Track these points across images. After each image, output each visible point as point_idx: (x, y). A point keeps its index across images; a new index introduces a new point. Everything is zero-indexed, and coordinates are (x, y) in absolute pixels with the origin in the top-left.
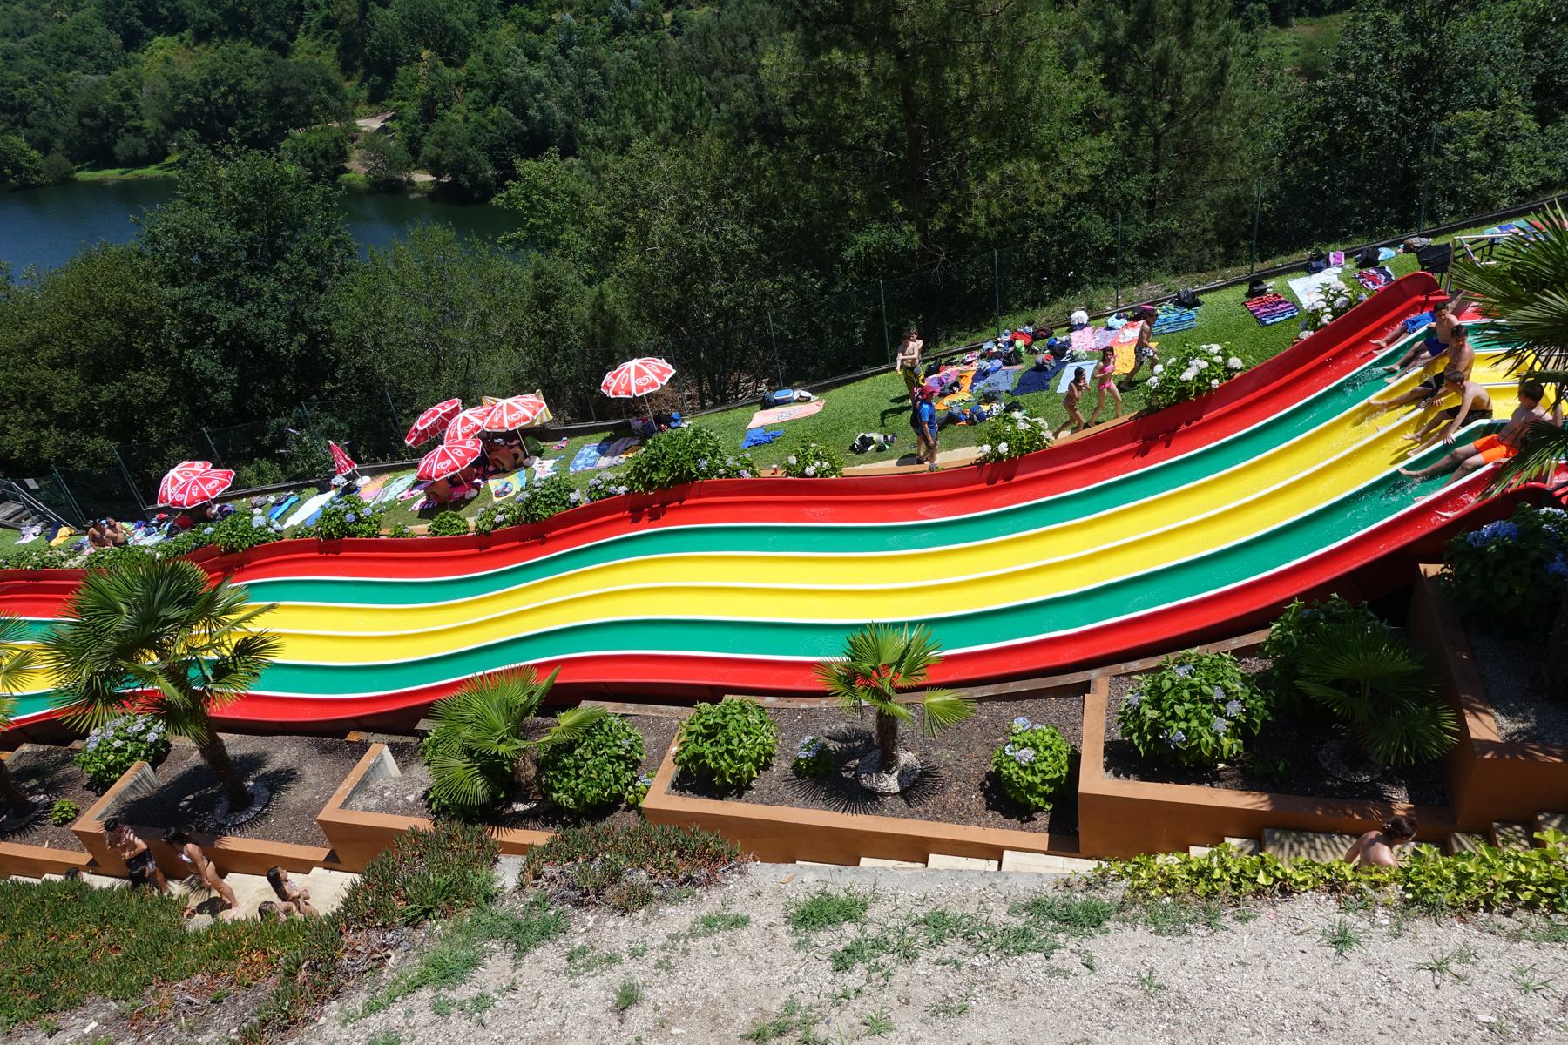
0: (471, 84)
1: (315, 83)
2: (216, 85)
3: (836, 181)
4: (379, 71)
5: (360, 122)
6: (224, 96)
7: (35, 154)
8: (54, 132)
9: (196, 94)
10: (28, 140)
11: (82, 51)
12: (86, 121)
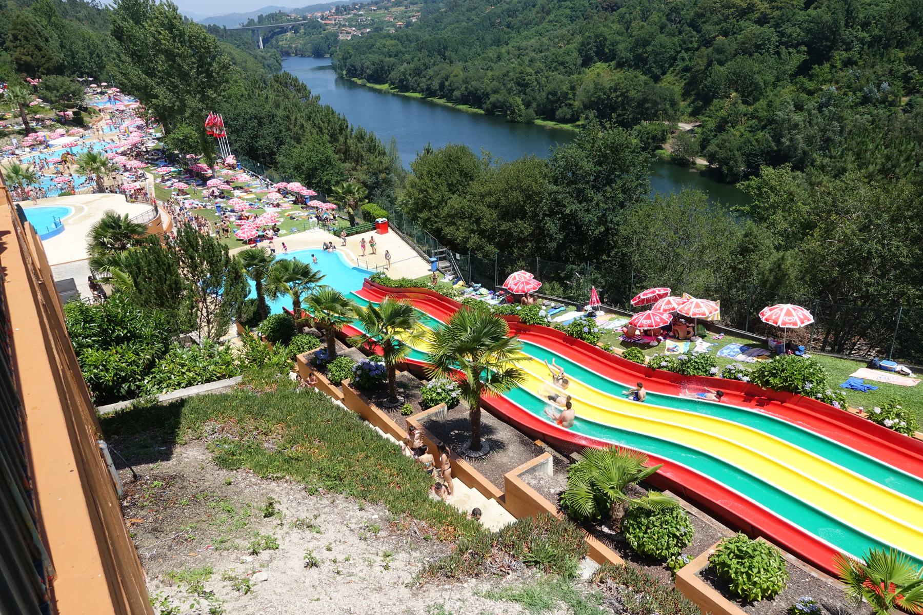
1: (665, 99)
2: (615, 91)
4: (701, 96)
5: (680, 125)
6: (617, 97)
7: (522, 107)
8: (534, 99)
12: (550, 97)
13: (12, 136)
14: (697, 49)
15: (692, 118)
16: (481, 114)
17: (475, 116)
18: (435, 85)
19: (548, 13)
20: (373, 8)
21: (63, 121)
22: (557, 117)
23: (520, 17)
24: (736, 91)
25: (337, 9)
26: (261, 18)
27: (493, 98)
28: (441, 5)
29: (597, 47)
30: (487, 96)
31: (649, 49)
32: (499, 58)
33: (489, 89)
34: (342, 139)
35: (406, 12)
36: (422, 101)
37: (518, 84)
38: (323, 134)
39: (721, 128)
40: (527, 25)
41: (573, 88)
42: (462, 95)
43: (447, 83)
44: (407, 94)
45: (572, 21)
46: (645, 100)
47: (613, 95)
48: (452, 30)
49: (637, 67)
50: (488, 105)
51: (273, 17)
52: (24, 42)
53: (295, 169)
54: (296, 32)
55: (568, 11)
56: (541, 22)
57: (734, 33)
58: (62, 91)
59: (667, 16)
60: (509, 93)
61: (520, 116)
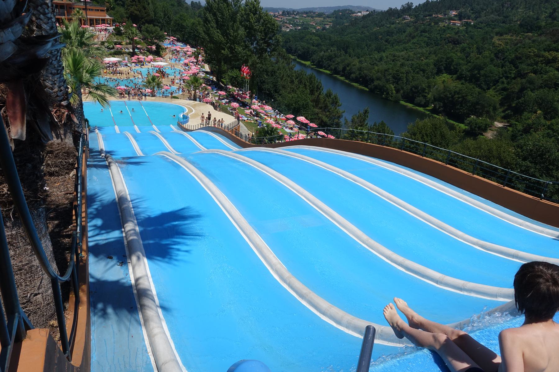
0: (549, 128)
1: (490, 105)
2: (458, 94)
3: (549, 165)
4: (513, 108)
5: (496, 123)
6: (459, 98)
7: (394, 92)
8: (402, 88)
9: (450, 94)
10: (395, 87)
11: (424, 71)
12: (413, 89)
13: (125, 55)
14: (514, 78)
15: (503, 120)
16: (366, 91)
17: (362, 91)
18: (340, 68)
19: (413, 38)
20: (305, 15)
21: (151, 52)
22: (415, 102)
23: (395, 37)
24: (540, 110)
25: (283, 12)
27: (376, 83)
28: (345, 21)
29: (446, 64)
30: (372, 80)
31: (482, 72)
32: (381, 59)
33: (374, 77)
34: (316, 94)
35: (323, 21)
36: (330, 76)
37: (394, 77)
38: (306, 89)
39: (527, 130)
40: (398, 42)
41: (429, 87)
42: (356, 77)
43: (348, 68)
44: (321, 70)
45: (428, 45)
46: (477, 103)
47: (457, 96)
48: (351, 37)
49: (470, 81)
50: (372, 86)
52: (137, 3)
53: (286, 106)
55: (426, 39)
56: (407, 42)
57: (541, 73)
58: (155, 34)
59: (495, 54)
60: (387, 82)
61: (392, 97)
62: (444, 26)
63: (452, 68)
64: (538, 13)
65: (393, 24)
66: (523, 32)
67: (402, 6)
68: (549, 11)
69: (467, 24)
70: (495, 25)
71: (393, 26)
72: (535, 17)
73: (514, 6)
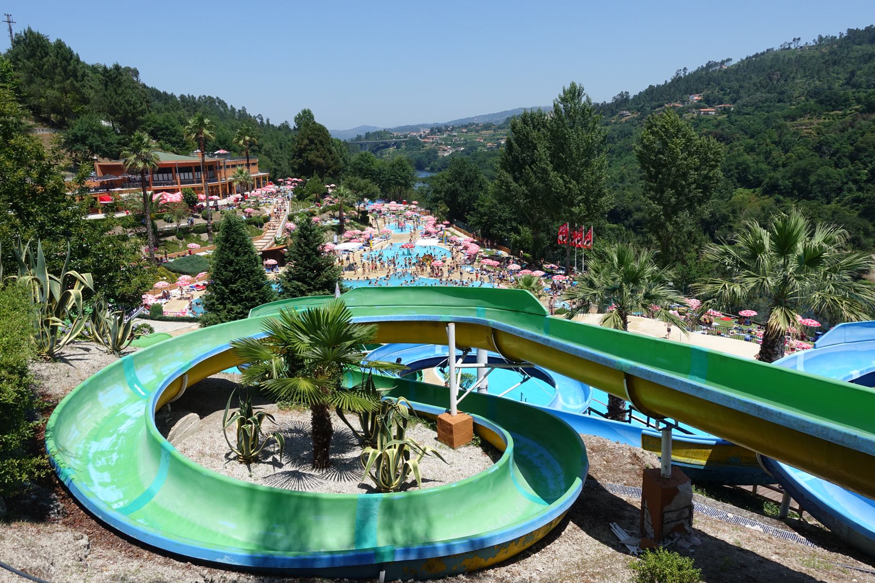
20: (464, 130)
26: (368, 135)
30: (629, 213)
33: (631, 207)
51: (378, 134)
52: (319, 146)
54: (398, 147)
62: (692, 118)
63: (751, 178)
64: (828, 81)
65: (607, 125)
66: (827, 110)
67: (614, 98)
68: (843, 76)
69: (726, 111)
70: (769, 107)
71: (609, 128)
72: (826, 87)
73: (788, 76)
